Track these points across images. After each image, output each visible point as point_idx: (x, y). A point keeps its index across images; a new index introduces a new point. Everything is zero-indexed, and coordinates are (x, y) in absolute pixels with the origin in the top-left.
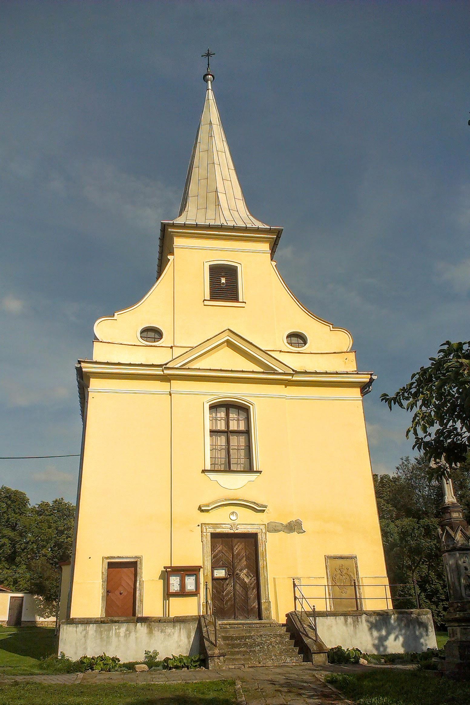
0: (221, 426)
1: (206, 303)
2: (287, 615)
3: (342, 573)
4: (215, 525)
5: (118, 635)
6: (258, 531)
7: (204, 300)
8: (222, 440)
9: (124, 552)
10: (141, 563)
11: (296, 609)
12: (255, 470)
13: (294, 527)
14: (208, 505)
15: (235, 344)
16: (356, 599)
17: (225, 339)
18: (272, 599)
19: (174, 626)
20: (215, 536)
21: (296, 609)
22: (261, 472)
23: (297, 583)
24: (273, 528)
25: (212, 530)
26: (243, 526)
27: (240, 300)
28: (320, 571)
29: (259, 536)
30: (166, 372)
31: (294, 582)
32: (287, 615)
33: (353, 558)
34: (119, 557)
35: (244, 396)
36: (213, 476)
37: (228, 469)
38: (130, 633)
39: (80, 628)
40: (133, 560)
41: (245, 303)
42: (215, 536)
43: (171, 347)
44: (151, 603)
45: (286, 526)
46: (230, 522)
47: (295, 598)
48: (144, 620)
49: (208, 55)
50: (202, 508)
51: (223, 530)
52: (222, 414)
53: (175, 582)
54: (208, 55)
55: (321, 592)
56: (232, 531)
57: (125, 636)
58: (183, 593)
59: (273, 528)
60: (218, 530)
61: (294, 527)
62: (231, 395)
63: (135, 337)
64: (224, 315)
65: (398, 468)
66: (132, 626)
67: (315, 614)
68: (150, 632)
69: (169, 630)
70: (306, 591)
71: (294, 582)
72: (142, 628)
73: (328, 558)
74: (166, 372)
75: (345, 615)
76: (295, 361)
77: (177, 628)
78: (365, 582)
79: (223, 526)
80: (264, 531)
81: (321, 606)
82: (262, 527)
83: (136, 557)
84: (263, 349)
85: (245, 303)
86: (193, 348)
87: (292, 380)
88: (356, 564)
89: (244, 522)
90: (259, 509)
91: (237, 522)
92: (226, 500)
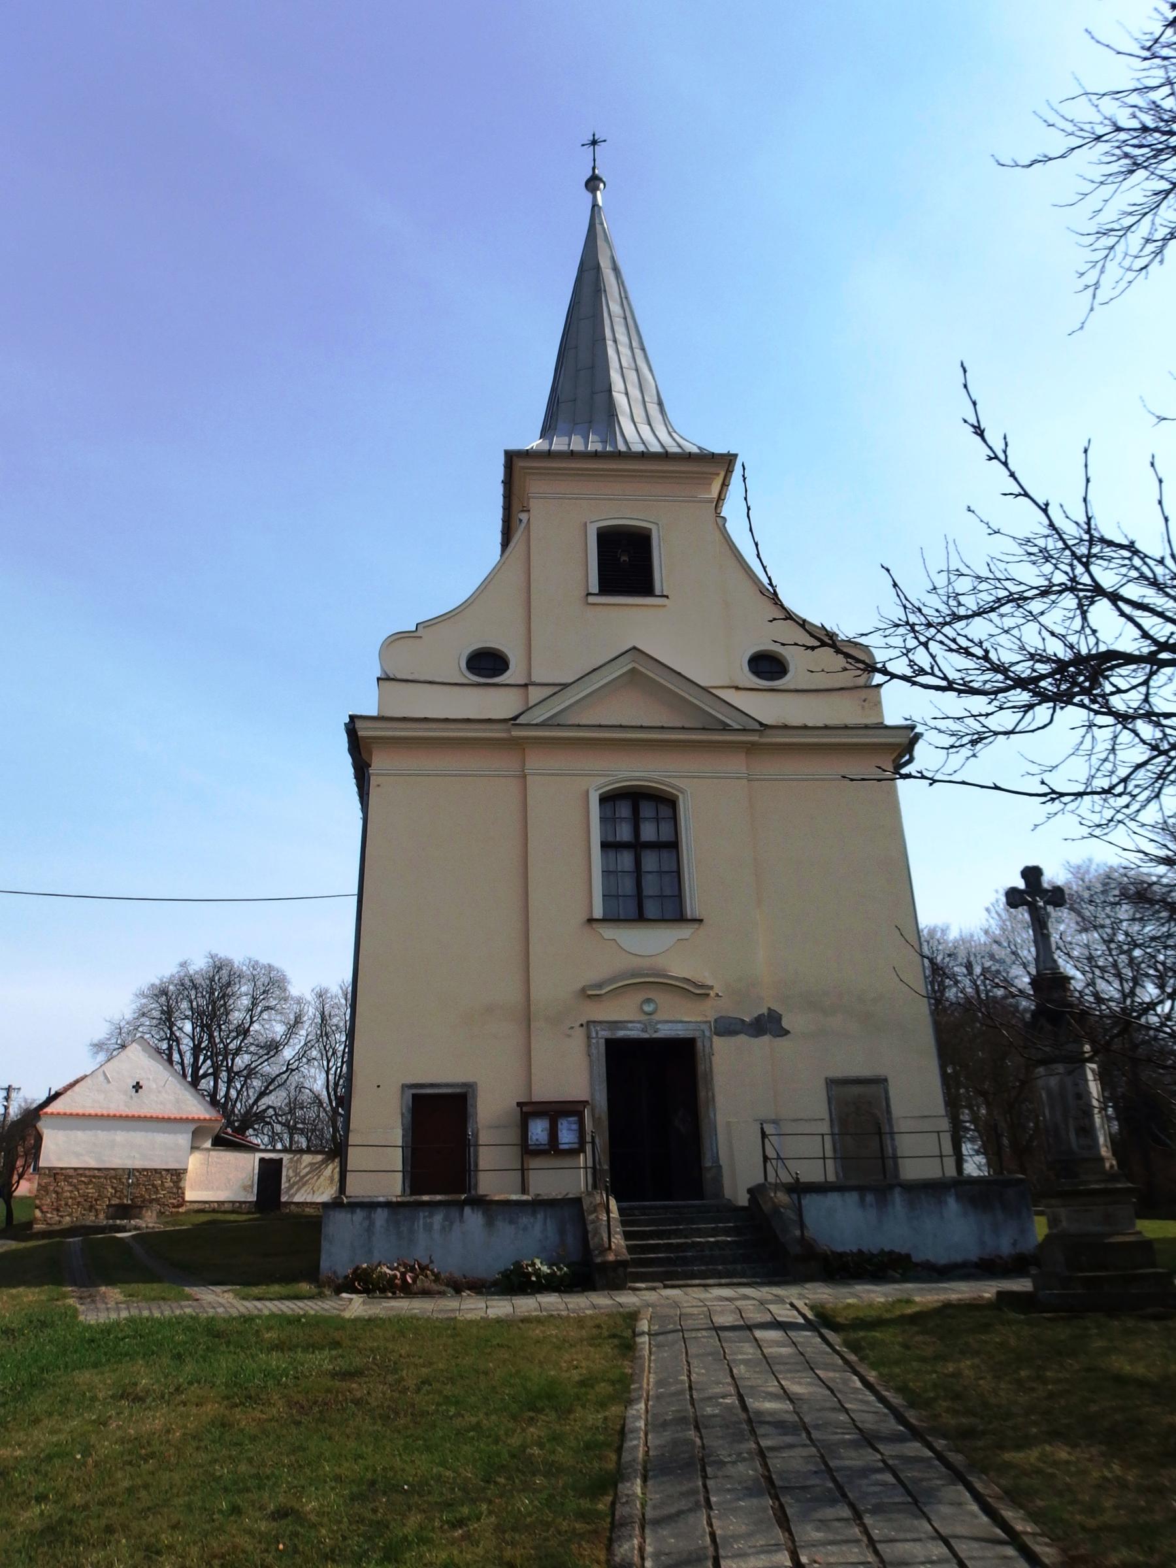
0: (624, 833)
1: (591, 599)
2: (750, 1191)
3: (859, 1112)
4: (615, 1025)
5: (428, 1228)
6: (697, 1034)
7: (589, 594)
8: (626, 860)
9: (441, 1071)
10: (475, 1097)
11: (766, 1179)
12: (689, 917)
13: (768, 1025)
14: (600, 986)
15: (640, 672)
16: (883, 1158)
17: (630, 666)
18: (724, 1160)
19: (534, 1214)
20: (611, 1044)
21: (766, 1179)
22: (701, 921)
23: (769, 1129)
24: (727, 1027)
25: (607, 1034)
26: (666, 1026)
27: (657, 592)
28: (814, 1106)
29: (699, 1044)
30: (516, 733)
31: (762, 1129)
32: (750, 1191)
33: (881, 1081)
34: (432, 1085)
35: (669, 777)
36: (609, 932)
37: (640, 917)
38: (452, 1223)
39: (359, 1215)
40: (458, 1090)
41: (667, 597)
42: (611, 1044)
43: (526, 685)
44: (494, 1174)
45: (751, 1024)
46: (644, 1018)
47: (766, 1159)
48: (480, 1203)
49: (594, 143)
50: (590, 993)
51: (628, 1033)
52: (624, 810)
53: (538, 1130)
54: (594, 143)
55: (812, 1147)
56: (646, 1036)
57: (443, 1228)
58: (553, 1148)
59: (727, 1027)
60: (621, 1034)
61: (768, 1025)
62: (642, 774)
63: (456, 668)
64: (632, 624)
65: (988, 910)
66: (454, 1212)
67: (798, 1189)
68: (490, 1223)
69: (524, 1220)
70: (790, 1147)
71: (762, 1129)
72: (473, 1219)
73: (831, 1083)
74: (516, 733)
75: (861, 1189)
76: (764, 707)
77: (540, 1216)
78: (901, 1125)
79: (630, 1025)
80: (707, 1033)
81: (811, 1173)
82: (704, 1027)
83: (464, 1085)
84: (702, 684)
85: (667, 597)
86: (565, 686)
87: (759, 742)
88: (886, 1092)
89: (673, 1019)
90: (696, 991)
91: (656, 1017)
92: (633, 976)
